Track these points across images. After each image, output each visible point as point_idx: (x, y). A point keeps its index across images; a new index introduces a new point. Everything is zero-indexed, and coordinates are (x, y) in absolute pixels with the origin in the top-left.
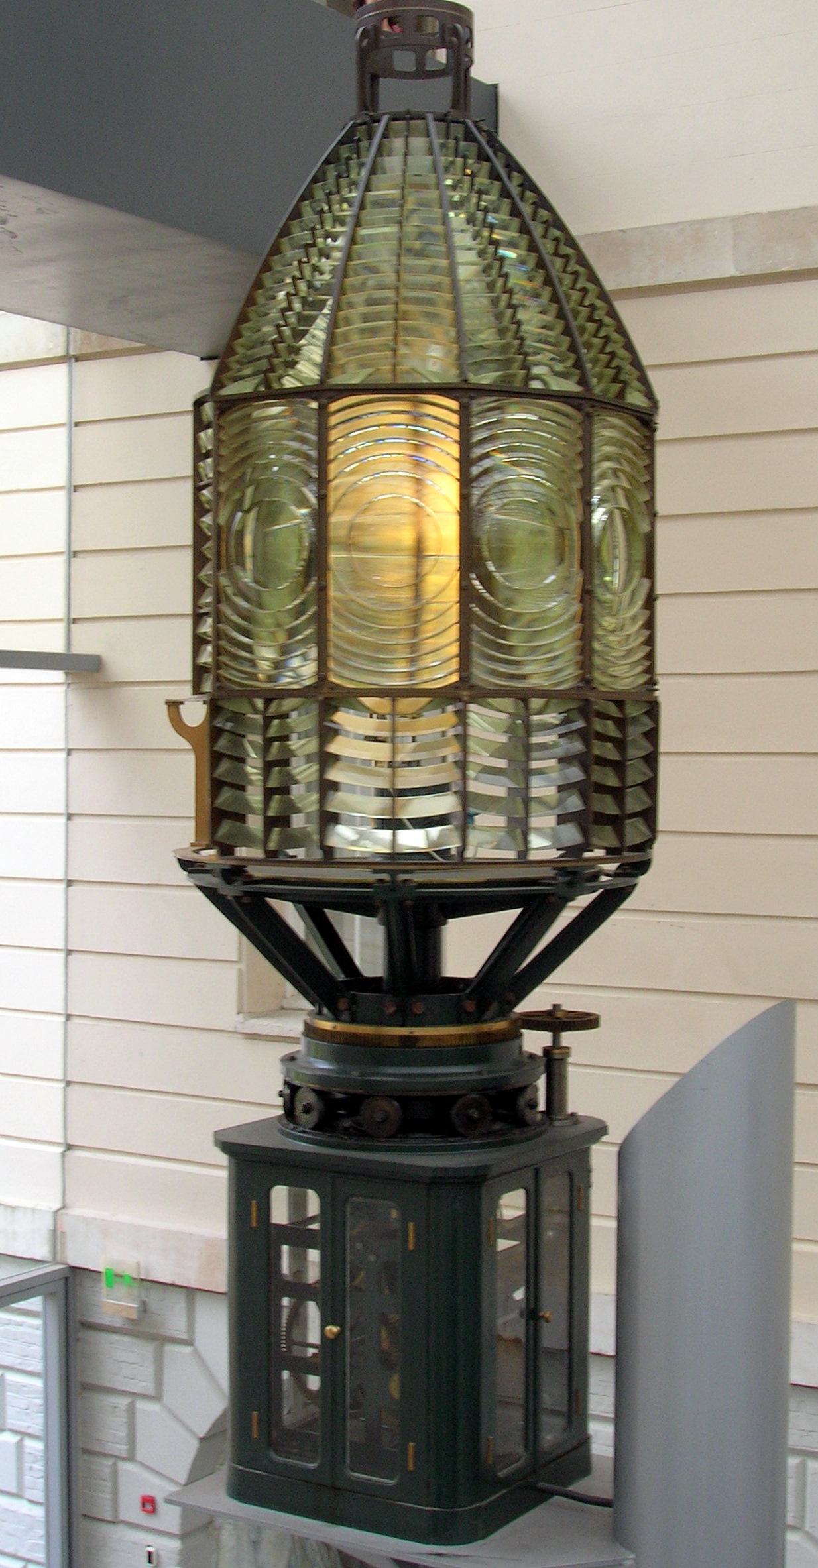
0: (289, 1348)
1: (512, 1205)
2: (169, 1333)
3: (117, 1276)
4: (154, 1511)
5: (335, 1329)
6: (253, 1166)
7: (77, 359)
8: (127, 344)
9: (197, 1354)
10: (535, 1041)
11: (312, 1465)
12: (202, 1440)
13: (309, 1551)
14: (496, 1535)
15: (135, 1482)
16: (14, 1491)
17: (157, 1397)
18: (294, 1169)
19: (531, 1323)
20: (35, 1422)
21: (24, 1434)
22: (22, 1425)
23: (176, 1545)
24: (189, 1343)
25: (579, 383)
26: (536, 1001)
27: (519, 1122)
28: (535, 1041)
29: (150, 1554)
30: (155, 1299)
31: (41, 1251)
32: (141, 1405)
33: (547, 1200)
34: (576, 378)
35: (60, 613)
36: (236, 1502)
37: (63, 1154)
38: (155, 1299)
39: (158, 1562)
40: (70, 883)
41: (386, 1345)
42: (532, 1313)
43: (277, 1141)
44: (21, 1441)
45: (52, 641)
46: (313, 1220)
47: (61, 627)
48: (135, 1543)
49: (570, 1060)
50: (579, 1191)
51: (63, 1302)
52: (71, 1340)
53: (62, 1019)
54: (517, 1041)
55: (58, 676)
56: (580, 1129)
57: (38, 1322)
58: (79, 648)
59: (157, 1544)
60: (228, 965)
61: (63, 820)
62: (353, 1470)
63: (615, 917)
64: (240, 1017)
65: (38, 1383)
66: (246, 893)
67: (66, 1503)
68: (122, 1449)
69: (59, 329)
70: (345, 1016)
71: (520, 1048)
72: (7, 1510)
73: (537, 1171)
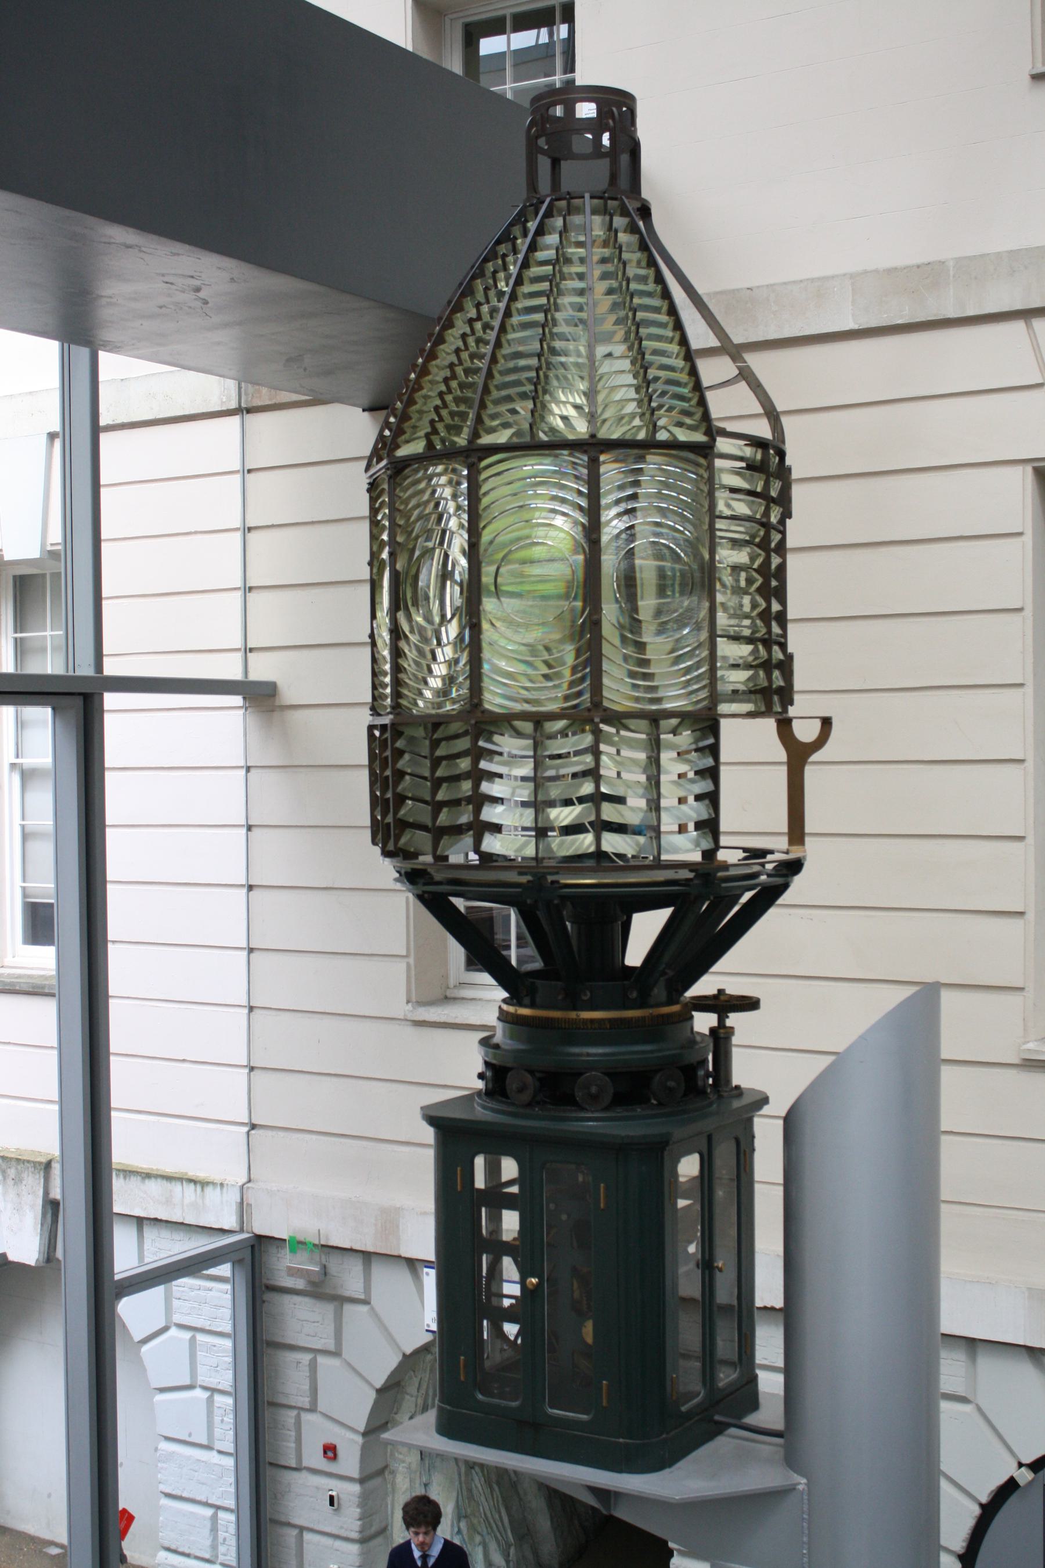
0: (488, 1298)
1: (689, 1167)
2: (347, 1294)
3: (300, 1243)
4: (335, 1458)
5: (534, 1280)
6: (456, 1136)
7: (249, 411)
8: (295, 397)
9: (375, 1314)
10: (703, 1022)
11: (515, 1404)
12: (379, 1391)
13: (475, 1491)
14: (681, 1464)
15: (316, 1432)
16: (205, 1443)
17: (336, 1353)
18: (494, 1140)
19: (707, 1272)
20: (225, 1379)
21: (213, 1390)
22: (212, 1382)
23: (356, 1488)
24: (366, 1302)
25: (705, 434)
26: (704, 986)
27: (702, 1092)
28: (703, 1022)
29: (332, 1498)
30: (335, 1264)
31: (229, 1221)
32: (321, 1360)
33: (718, 1162)
34: (703, 429)
35: (238, 643)
36: (445, 1439)
37: (248, 1133)
38: (335, 1264)
39: (339, 1504)
40: (250, 888)
41: (577, 1294)
42: (707, 1265)
43: (481, 1113)
44: (211, 1397)
45: (230, 669)
46: (511, 1183)
47: (239, 656)
48: (317, 1488)
49: (735, 1040)
50: (745, 1154)
51: (250, 1268)
52: (258, 1303)
53: (246, 1011)
54: (689, 1023)
55: (237, 700)
56: (745, 1101)
57: (228, 1287)
58: (254, 676)
59: (337, 1488)
60: (398, 959)
61: (244, 830)
62: (551, 1408)
63: (772, 911)
64: (410, 1006)
65: (228, 1343)
66: (424, 892)
67: (253, 1452)
68: (305, 1401)
69: (53, 347)
70: (527, 1000)
71: (692, 1028)
72: (199, 1460)
73: (710, 1138)
